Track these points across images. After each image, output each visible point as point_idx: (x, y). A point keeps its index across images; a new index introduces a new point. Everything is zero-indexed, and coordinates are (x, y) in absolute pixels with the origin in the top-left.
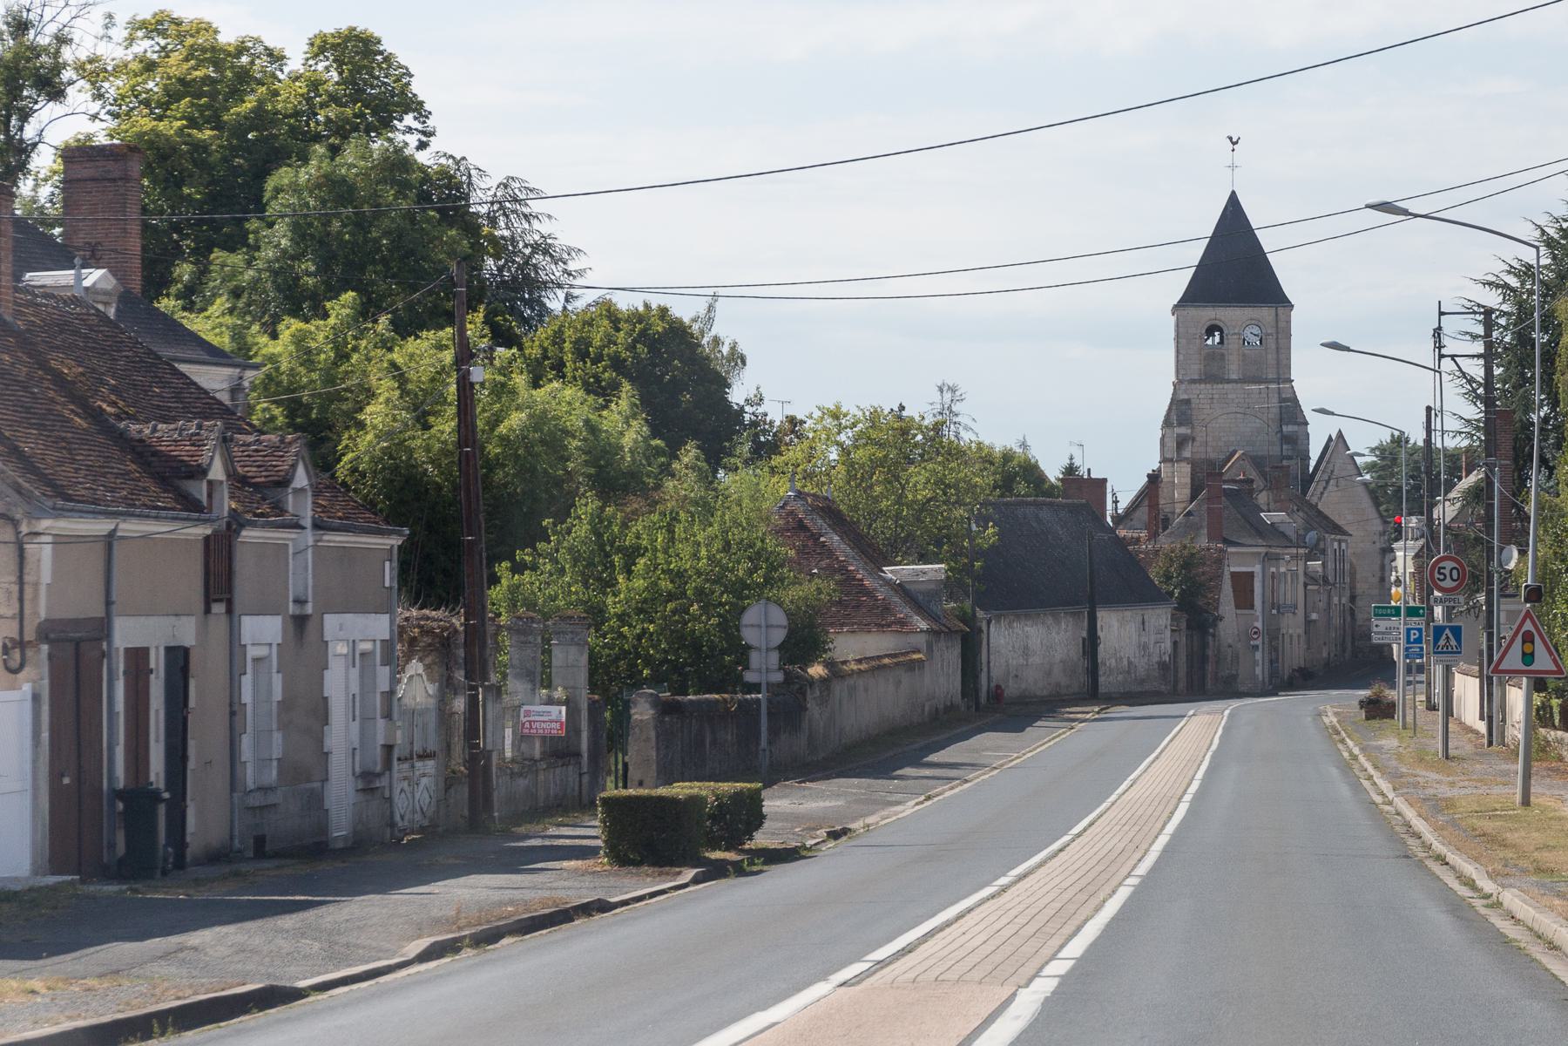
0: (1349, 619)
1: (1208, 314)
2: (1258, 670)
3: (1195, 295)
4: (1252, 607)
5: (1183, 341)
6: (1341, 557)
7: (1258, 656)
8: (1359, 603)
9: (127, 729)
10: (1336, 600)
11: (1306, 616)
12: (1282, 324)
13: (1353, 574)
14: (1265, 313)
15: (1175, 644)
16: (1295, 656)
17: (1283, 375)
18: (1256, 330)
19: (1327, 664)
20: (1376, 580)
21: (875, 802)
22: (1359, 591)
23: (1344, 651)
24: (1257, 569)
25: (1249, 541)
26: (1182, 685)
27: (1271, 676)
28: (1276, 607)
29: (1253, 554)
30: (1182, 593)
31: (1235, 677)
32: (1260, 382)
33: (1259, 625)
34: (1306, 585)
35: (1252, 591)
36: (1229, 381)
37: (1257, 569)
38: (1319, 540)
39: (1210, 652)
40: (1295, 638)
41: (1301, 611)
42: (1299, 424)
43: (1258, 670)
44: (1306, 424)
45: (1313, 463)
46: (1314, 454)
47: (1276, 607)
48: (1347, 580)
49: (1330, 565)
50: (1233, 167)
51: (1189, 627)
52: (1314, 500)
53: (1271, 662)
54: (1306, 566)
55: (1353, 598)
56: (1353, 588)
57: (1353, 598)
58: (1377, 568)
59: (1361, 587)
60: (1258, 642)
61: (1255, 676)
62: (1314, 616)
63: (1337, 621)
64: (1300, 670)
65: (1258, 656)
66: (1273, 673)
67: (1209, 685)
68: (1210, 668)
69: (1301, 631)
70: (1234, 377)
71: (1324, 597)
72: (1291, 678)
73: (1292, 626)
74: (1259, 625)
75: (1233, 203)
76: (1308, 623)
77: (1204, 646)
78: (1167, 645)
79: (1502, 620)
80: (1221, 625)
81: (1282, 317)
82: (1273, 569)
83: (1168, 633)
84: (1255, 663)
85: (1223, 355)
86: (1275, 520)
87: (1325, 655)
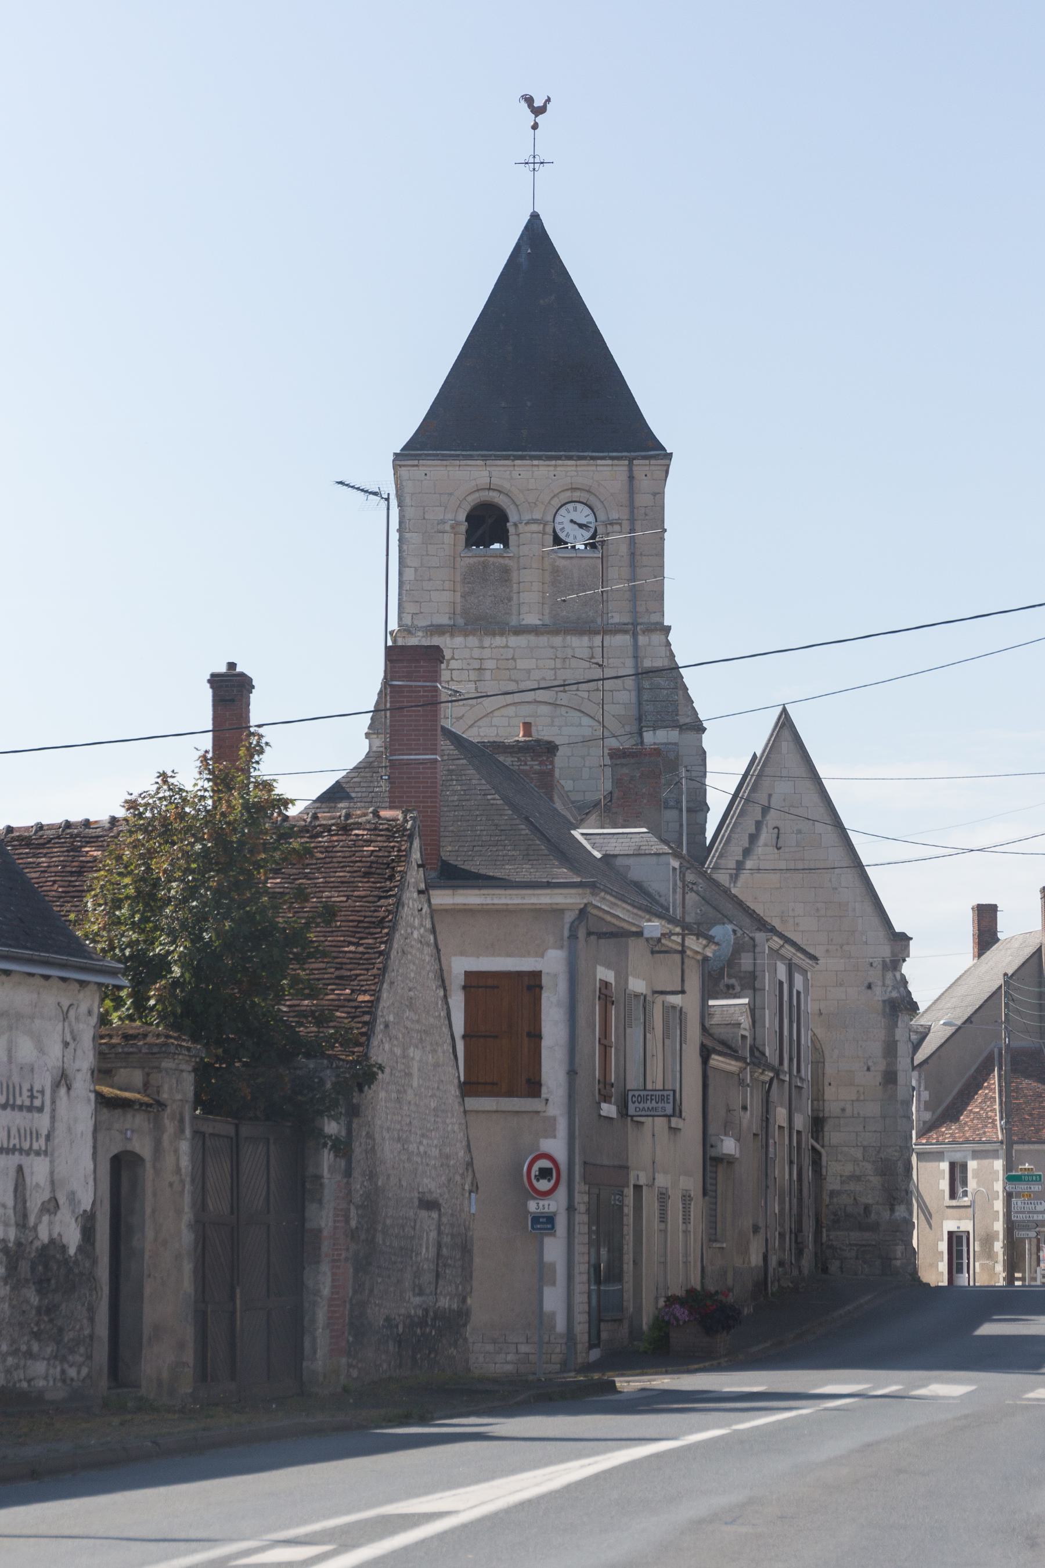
0: (809, 1173)
1: (471, 478)
2: (553, 1300)
3: (444, 433)
4: (534, 1087)
5: (411, 537)
6: (791, 1009)
7: (554, 1249)
8: (833, 1136)
9: (757, 1427)
10: (781, 1114)
11: (706, 1142)
12: (643, 500)
13: (819, 1064)
14: (605, 475)
15: (122, 1171)
16: (672, 1254)
17: (646, 621)
18: (583, 515)
19: (761, 1284)
20: (875, 1078)
21: (346, 1546)
22: (832, 1108)
23: (800, 1253)
24: (551, 963)
25: (525, 872)
26: (166, 1354)
27: (598, 1317)
28: (614, 1101)
29: (538, 912)
30: (202, 963)
31: (454, 1322)
32: (592, 632)
33: (556, 1146)
34: (705, 1054)
35: (536, 1036)
36: (521, 630)
37: (551, 963)
38: (738, 949)
39: (324, 1217)
40: (675, 1206)
41: (691, 1123)
42: (682, 728)
43: (553, 1300)
44: (699, 728)
45: (709, 834)
46: (720, 788)
47: (614, 1101)
48: (807, 1072)
49: (769, 1019)
50: (534, 163)
51: (210, 1099)
52: (722, 878)
53: (597, 1275)
54: (705, 1012)
55: (818, 1123)
56: (818, 1097)
57: (818, 1123)
58: (876, 1048)
59: (836, 1098)
60: (555, 1205)
61: (541, 1320)
62: (729, 1146)
63: (782, 1173)
64: (692, 1299)
65: (554, 1249)
66: (605, 1310)
67: (322, 1351)
68: (325, 1281)
69: (692, 1183)
70: (531, 619)
71: (753, 1099)
72: (662, 1325)
73: (665, 1162)
74: (556, 1146)
75: (535, 240)
76: (713, 1163)
77: (301, 1188)
78: (73, 1170)
79: (977, 1270)
80: (381, 1097)
81: (644, 484)
82: (606, 974)
83: (78, 1112)
84: (542, 1274)
85: (506, 570)
86: (615, 847)
87: (755, 1259)
